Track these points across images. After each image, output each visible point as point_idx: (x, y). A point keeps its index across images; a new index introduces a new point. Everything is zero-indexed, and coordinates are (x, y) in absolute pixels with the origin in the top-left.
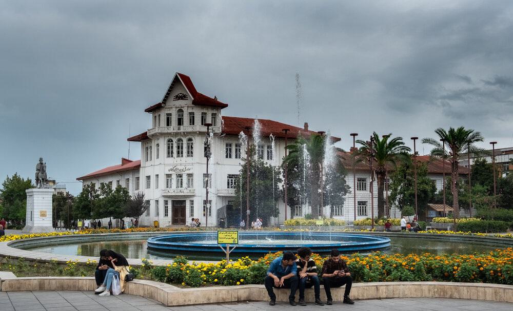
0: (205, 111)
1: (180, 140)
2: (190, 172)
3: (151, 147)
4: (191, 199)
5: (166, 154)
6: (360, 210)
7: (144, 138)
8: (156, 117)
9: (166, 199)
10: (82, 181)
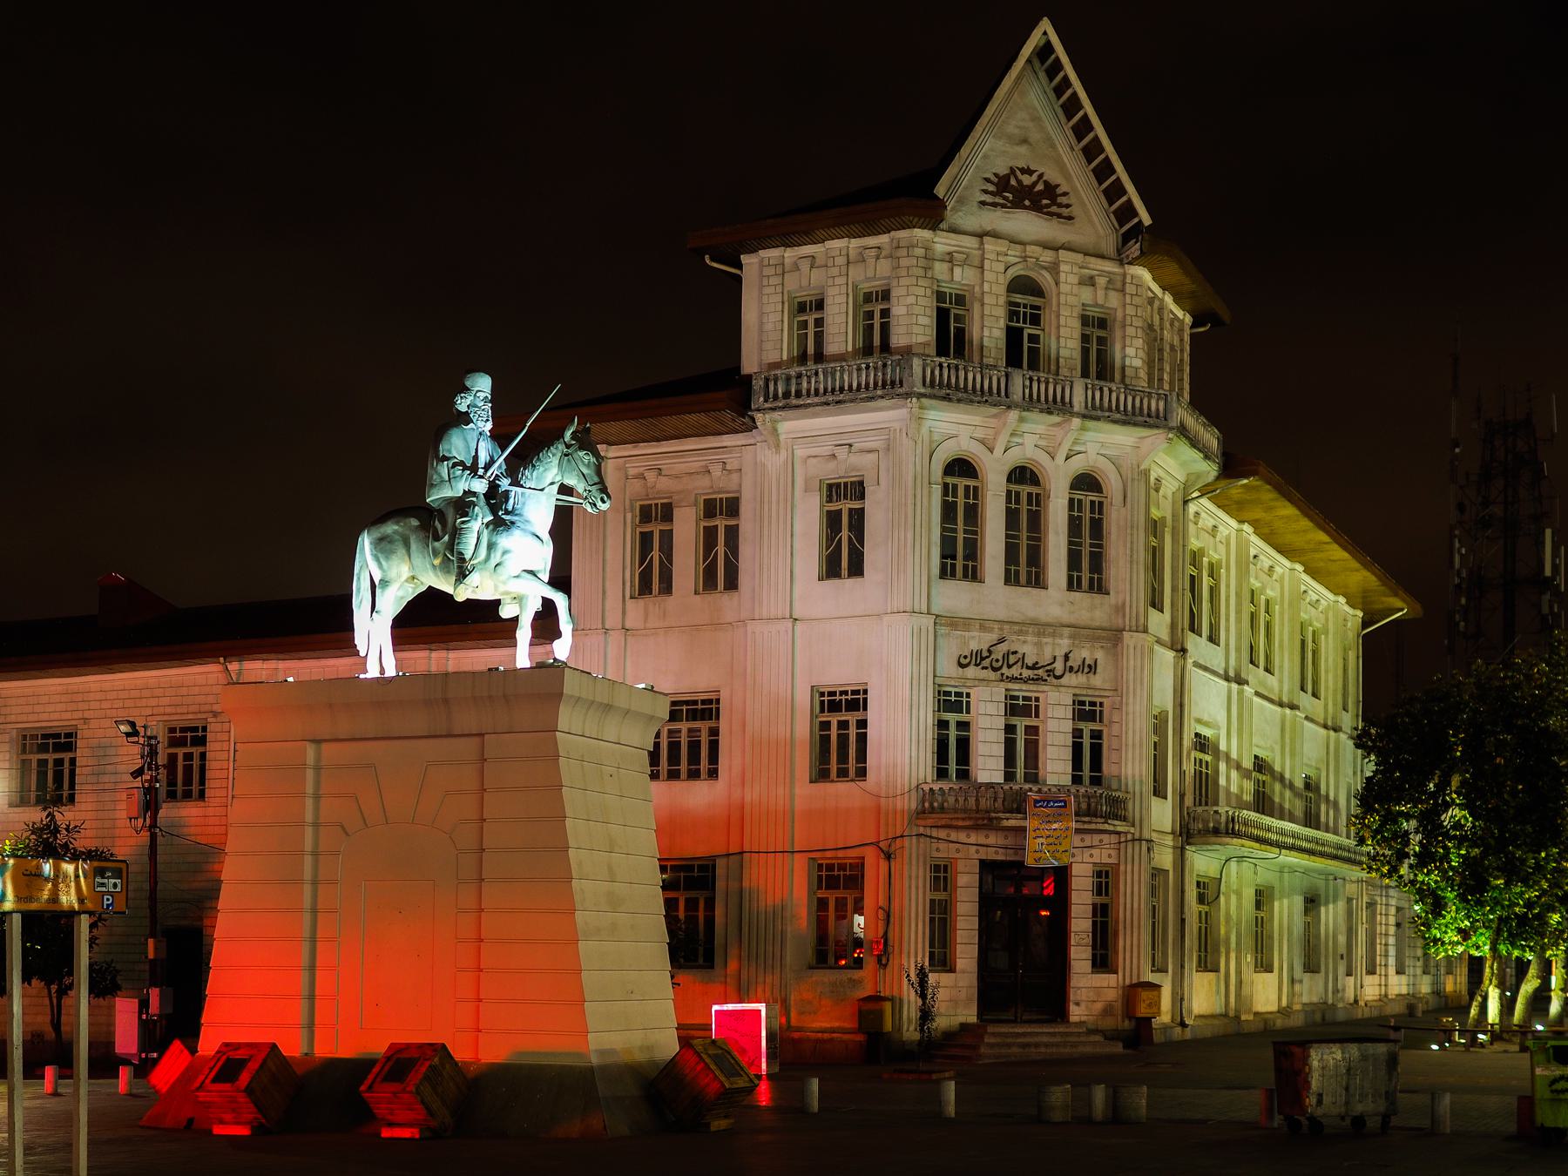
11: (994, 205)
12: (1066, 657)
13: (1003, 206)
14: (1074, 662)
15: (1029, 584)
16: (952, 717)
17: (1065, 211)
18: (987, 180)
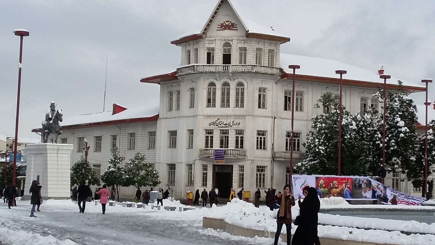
0: (261, 46)
1: (226, 84)
2: (240, 127)
3: (179, 92)
4: (241, 164)
5: (205, 103)
6: (260, 178)
7: (167, 80)
8: (189, 52)
9: (205, 163)
10: (40, 133)
11: (220, 30)
12: (233, 122)
13: (222, 30)
14: (235, 123)
15: (227, 107)
16: (209, 135)
17: (236, 29)
18: (219, 25)
